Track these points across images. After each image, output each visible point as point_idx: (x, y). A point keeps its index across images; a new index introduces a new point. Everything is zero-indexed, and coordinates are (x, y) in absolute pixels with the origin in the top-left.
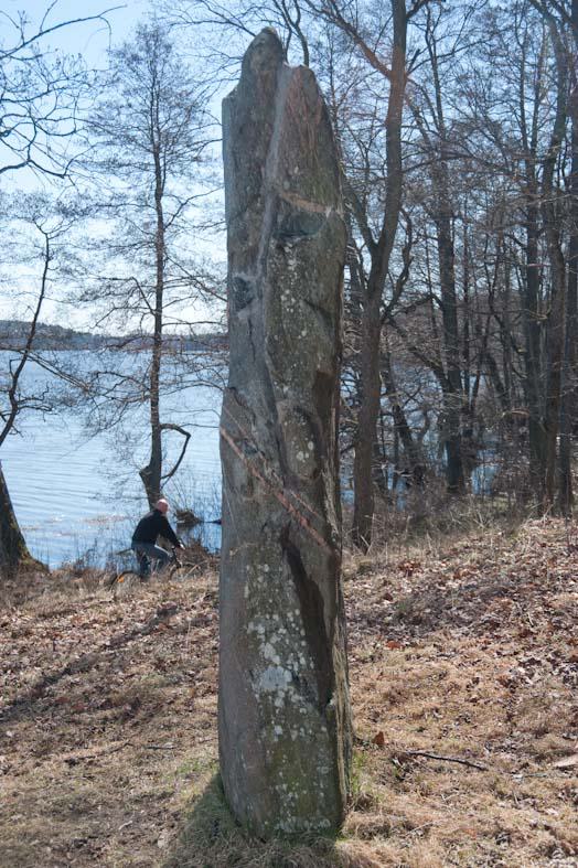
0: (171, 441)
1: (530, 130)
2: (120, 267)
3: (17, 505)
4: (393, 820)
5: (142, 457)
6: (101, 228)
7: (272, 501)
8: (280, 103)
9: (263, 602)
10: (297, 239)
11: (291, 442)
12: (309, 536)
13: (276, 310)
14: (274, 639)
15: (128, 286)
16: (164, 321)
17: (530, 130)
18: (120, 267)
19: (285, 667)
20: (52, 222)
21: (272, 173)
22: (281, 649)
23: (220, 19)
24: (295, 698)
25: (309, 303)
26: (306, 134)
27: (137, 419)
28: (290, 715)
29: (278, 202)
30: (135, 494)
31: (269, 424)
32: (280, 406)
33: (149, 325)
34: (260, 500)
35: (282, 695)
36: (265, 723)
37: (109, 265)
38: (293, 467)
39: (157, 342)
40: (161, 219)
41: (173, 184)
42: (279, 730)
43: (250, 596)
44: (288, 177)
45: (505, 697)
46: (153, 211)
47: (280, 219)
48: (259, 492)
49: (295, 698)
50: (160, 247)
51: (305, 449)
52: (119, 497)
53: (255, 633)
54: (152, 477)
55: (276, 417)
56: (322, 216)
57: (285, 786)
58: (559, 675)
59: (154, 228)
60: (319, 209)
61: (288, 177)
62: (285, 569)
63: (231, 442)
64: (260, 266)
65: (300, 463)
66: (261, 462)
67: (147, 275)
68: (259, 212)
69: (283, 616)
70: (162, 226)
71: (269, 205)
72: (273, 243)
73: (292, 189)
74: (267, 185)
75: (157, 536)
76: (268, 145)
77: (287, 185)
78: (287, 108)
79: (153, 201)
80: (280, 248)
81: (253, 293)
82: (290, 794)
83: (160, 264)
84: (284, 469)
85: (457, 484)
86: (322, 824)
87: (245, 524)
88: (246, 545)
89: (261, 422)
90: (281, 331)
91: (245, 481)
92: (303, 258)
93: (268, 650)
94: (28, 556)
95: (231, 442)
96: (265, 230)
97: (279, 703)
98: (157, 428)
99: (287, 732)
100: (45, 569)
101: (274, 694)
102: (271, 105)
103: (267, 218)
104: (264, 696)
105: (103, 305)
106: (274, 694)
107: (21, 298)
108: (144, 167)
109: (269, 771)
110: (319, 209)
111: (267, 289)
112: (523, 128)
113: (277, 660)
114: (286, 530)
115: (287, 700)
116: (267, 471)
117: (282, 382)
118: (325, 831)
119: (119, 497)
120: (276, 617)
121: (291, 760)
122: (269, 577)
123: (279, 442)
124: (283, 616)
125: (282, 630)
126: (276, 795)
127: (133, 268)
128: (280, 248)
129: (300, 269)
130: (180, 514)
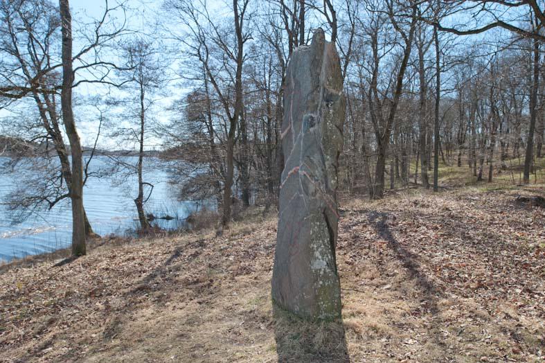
0: (146, 189)
1: (267, 85)
2: (126, 124)
3: (90, 214)
4: (354, 311)
5: (135, 195)
6: (119, 110)
7: (321, 198)
8: (325, 54)
9: (317, 236)
10: (332, 103)
11: (330, 177)
12: (332, 211)
13: (325, 128)
14: (320, 249)
15: (130, 131)
16: (144, 144)
17: (267, 85)
18: (126, 124)
19: (323, 259)
20: (104, 106)
21: (323, 78)
22: (322, 254)
23: (172, 37)
24: (328, 271)
25: (336, 126)
26: (334, 65)
27: (133, 181)
28: (326, 277)
29: (324, 89)
30: (131, 208)
31: (323, 170)
32: (326, 163)
33: (138, 148)
34: (318, 198)
35: (323, 270)
36: (316, 281)
37: (123, 123)
38: (330, 186)
39: (142, 154)
40: (143, 107)
41: (146, 95)
42: (321, 282)
43: (313, 234)
44: (328, 80)
45: (351, 268)
46: (140, 105)
47: (325, 95)
48: (318, 195)
49: (328, 271)
50: (142, 117)
51: (334, 179)
52: (125, 209)
53: (313, 247)
54: (139, 202)
55: (325, 167)
56: (338, 95)
57: (322, 303)
58: (347, 263)
59: (140, 111)
60: (337, 92)
61: (328, 80)
62: (325, 224)
63: (308, 177)
64: (318, 112)
65: (332, 184)
66: (320, 184)
67: (137, 128)
68: (319, 92)
69: (323, 241)
70: (143, 111)
71: (322, 88)
72: (325, 103)
73: (330, 85)
74: (321, 83)
75: (147, 226)
76: (321, 68)
77: (328, 83)
78: (328, 55)
79: (140, 101)
80: (327, 105)
81: (316, 121)
82: (324, 305)
83: (143, 123)
84: (327, 186)
85: (247, 204)
86: (335, 315)
87: (312, 207)
88: (312, 215)
89: (320, 169)
90: (327, 136)
91: (314, 191)
92: (334, 109)
93: (317, 254)
94: (92, 231)
95: (308, 177)
96: (321, 98)
97: (322, 273)
98: (141, 184)
99: (324, 283)
100: (99, 237)
101: (320, 270)
102: (322, 54)
103: (321, 94)
104: (316, 271)
105: (119, 138)
106: (320, 270)
107: (90, 135)
108: (137, 89)
109: (316, 297)
110: (337, 92)
111: (322, 120)
112: (266, 84)
113: (320, 257)
114: (325, 209)
115: (325, 272)
116: (322, 187)
117: (327, 155)
118: (337, 317)
119: (125, 209)
120: (321, 241)
121: (325, 293)
122: (319, 227)
123: (326, 177)
124: (323, 241)
125: (323, 246)
126: (319, 306)
127: (132, 125)
128: (327, 105)
129: (334, 113)
130: (149, 216)
